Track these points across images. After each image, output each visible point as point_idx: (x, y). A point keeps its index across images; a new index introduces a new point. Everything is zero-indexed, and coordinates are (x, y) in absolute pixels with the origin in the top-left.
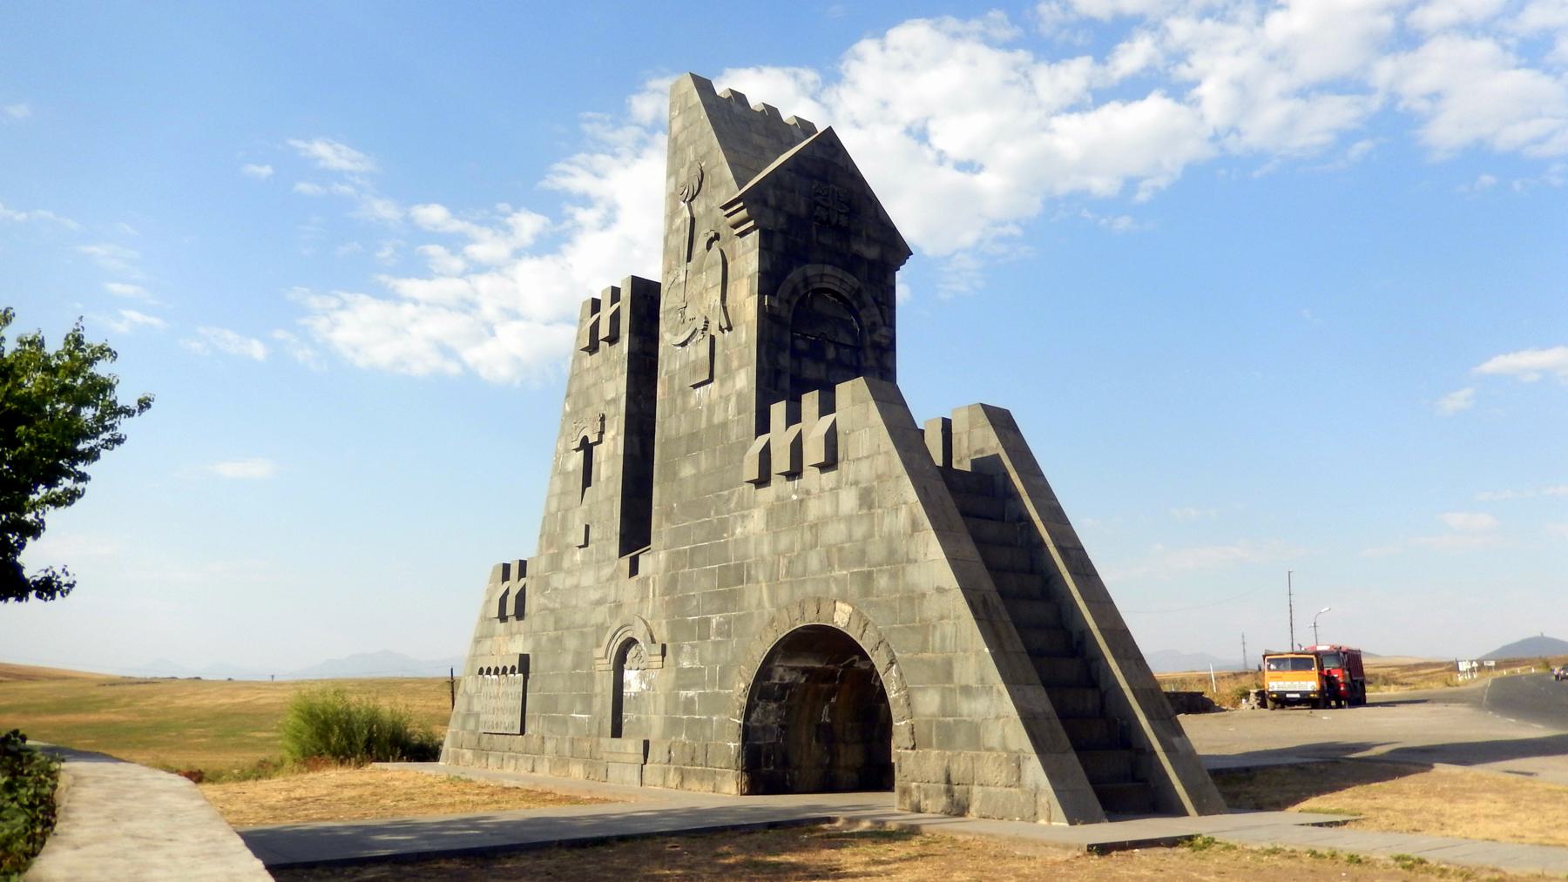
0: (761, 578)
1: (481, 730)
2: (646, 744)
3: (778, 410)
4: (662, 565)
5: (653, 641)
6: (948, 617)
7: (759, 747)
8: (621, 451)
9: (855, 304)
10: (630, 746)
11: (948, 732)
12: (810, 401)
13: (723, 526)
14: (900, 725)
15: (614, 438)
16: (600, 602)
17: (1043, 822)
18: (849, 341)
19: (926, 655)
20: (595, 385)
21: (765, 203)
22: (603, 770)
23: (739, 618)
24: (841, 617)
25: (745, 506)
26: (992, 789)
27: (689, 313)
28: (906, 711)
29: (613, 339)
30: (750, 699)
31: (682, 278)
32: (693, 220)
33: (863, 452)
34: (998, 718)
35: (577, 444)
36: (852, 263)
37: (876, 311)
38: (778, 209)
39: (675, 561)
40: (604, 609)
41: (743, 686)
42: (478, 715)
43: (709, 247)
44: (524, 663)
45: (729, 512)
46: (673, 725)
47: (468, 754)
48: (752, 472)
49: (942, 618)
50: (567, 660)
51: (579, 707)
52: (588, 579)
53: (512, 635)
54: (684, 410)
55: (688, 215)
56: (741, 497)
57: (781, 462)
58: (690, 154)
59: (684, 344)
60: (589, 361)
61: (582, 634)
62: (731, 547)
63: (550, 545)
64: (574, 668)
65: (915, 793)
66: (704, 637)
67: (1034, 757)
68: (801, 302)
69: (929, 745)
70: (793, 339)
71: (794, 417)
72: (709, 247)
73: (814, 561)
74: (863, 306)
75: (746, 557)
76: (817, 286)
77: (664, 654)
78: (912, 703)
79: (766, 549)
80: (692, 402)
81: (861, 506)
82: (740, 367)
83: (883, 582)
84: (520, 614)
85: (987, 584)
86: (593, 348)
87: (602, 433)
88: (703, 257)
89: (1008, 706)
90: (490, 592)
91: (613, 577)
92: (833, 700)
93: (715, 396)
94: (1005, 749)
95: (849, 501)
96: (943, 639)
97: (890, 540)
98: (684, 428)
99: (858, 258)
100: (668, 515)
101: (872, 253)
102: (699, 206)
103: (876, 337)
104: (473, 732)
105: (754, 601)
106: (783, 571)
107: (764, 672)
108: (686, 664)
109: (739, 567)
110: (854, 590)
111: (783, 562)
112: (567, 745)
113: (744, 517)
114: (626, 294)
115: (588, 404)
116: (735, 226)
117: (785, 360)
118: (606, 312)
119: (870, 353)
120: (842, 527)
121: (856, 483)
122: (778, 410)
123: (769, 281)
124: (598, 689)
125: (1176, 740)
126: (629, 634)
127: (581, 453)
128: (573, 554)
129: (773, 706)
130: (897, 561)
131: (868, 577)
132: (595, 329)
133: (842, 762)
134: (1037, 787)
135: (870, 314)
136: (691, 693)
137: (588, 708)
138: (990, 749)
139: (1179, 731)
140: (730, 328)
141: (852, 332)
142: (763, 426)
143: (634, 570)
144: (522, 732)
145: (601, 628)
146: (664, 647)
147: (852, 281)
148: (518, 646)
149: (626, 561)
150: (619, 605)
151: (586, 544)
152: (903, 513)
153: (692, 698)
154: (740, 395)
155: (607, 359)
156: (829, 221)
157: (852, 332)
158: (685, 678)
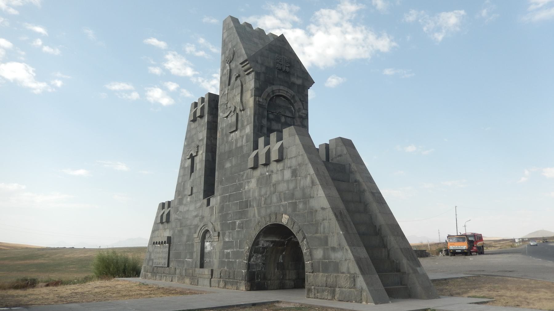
0: (255, 205)
1: (154, 265)
2: (212, 271)
3: (261, 140)
4: (219, 201)
5: (215, 231)
6: (326, 219)
7: (254, 272)
8: (204, 159)
9: (292, 101)
10: (206, 271)
11: (329, 266)
12: (273, 137)
13: (241, 186)
14: (307, 263)
15: (202, 154)
16: (196, 216)
17: (364, 303)
18: (290, 115)
19: (318, 235)
20: (195, 134)
21: (257, 62)
22: (196, 281)
23: (246, 221)
24: (285, 220)
25: (249, 178)
26: (344, 289)
27: (229, 105)
28: (310, 258)
29: (201, 117)
30: (251, 253)
31: (226, 92)
32: (231, 70)
33: (293, 155)
34: (346, 260)
35: (188, 157)
36: (291, 86)
37: (300, 104)
38: (262, 64)
39: (223, 200)
40: (198, 219)
41: (247, 248)
42: (153, 260)
43: (236, 80)
44: (169, 239)
45: (243, 180)
46: (222, 263)
47: (149, 275)
48: (251, 164)
49: (324, 220)
50: (184, 239)
51: (188, 257)
52: (192, 207)
53: (165, 229)
54: (227, 142)
55: (229, 68)
56: (248, 174)
57: (262, 160)
58: (230, 46)
59: (227, 117)
60: (193, 125)
61: (190, 228)
62: (243, 194)
63: (178, 196)
64: (187, 242)
65: (313, 290)
66: (233, 229)
67: (361, 276)
68: (271, 99)
69: (319, 271)
70: (268, 114)
71: (267, 143)
72: (236, 80)
73: (275, 199)
74: (295, 102)
75: (249, 197)
76: (277, 94)
77: (219, 236)
78: (313, 254)
79: (256, 194)
80: (230, 139)
81: (292, 177)
82: (247, 124)
83: (301, 206)
84: (168, 221)
85: (342, 206)
86: (194, 120)
87: (197, 152)
88: (234, 84)
89: (350, 255)
90: (158, 213)
91: (201, 207)
92: (284, 253)
93: (238, 136)
94: (349, 273)
95: (288, 174)
96: (324, 228)
97: (303, 189)
98: (227, 148)
99: (294, 84)
100: (221, 182)
101: (299, 82)
102: (233, 65)
103: (300, 114)
104: (151, 266)
105: (252, 215)
106: (263, 203)
107: (256, 242)
108: (227, 240)
109: (246, 201)
110: (289, 210)
111: (263, 199)
112: (184, 271)
113: (248, 182)
114: (206, 99)
115: (193, 141)
116: (245, 71)
117: (265, 122)
118: (200, 106)
119: (298, 120)
120: (285, 185)
121: (290, 167)
122: (261, 140)
123: (258, 92)
124: (195, 249)
125: (418, 269)
126: (206, 228)
127: (190, 160)
128: (187, 198)
129: (260, 255)
130: (306, 198)
131: (295, 205)
132: (195, 113)
133: (287, 278)
134: (362, 288)
135: (298, 105)
136: (229, 251)
137: (191, 257)
138: (343, 273)
139: (419, 265)
140: (243, 110)
141: (291, 112)
142: (256, 147)
143: (208, 204)
144: (168, 266)
145: (197, 226)
146: (219, 233)
147: (292, 92)
148: (167, 233)
149: (205, 201)
150: (203, 217)
151: (191, 194)
152: (309, 179)
153: (229, 253)
154: (247, 135)
155: (199, 124)
156: (281, 70)
157: (291, 112)
158: (227, 245)
